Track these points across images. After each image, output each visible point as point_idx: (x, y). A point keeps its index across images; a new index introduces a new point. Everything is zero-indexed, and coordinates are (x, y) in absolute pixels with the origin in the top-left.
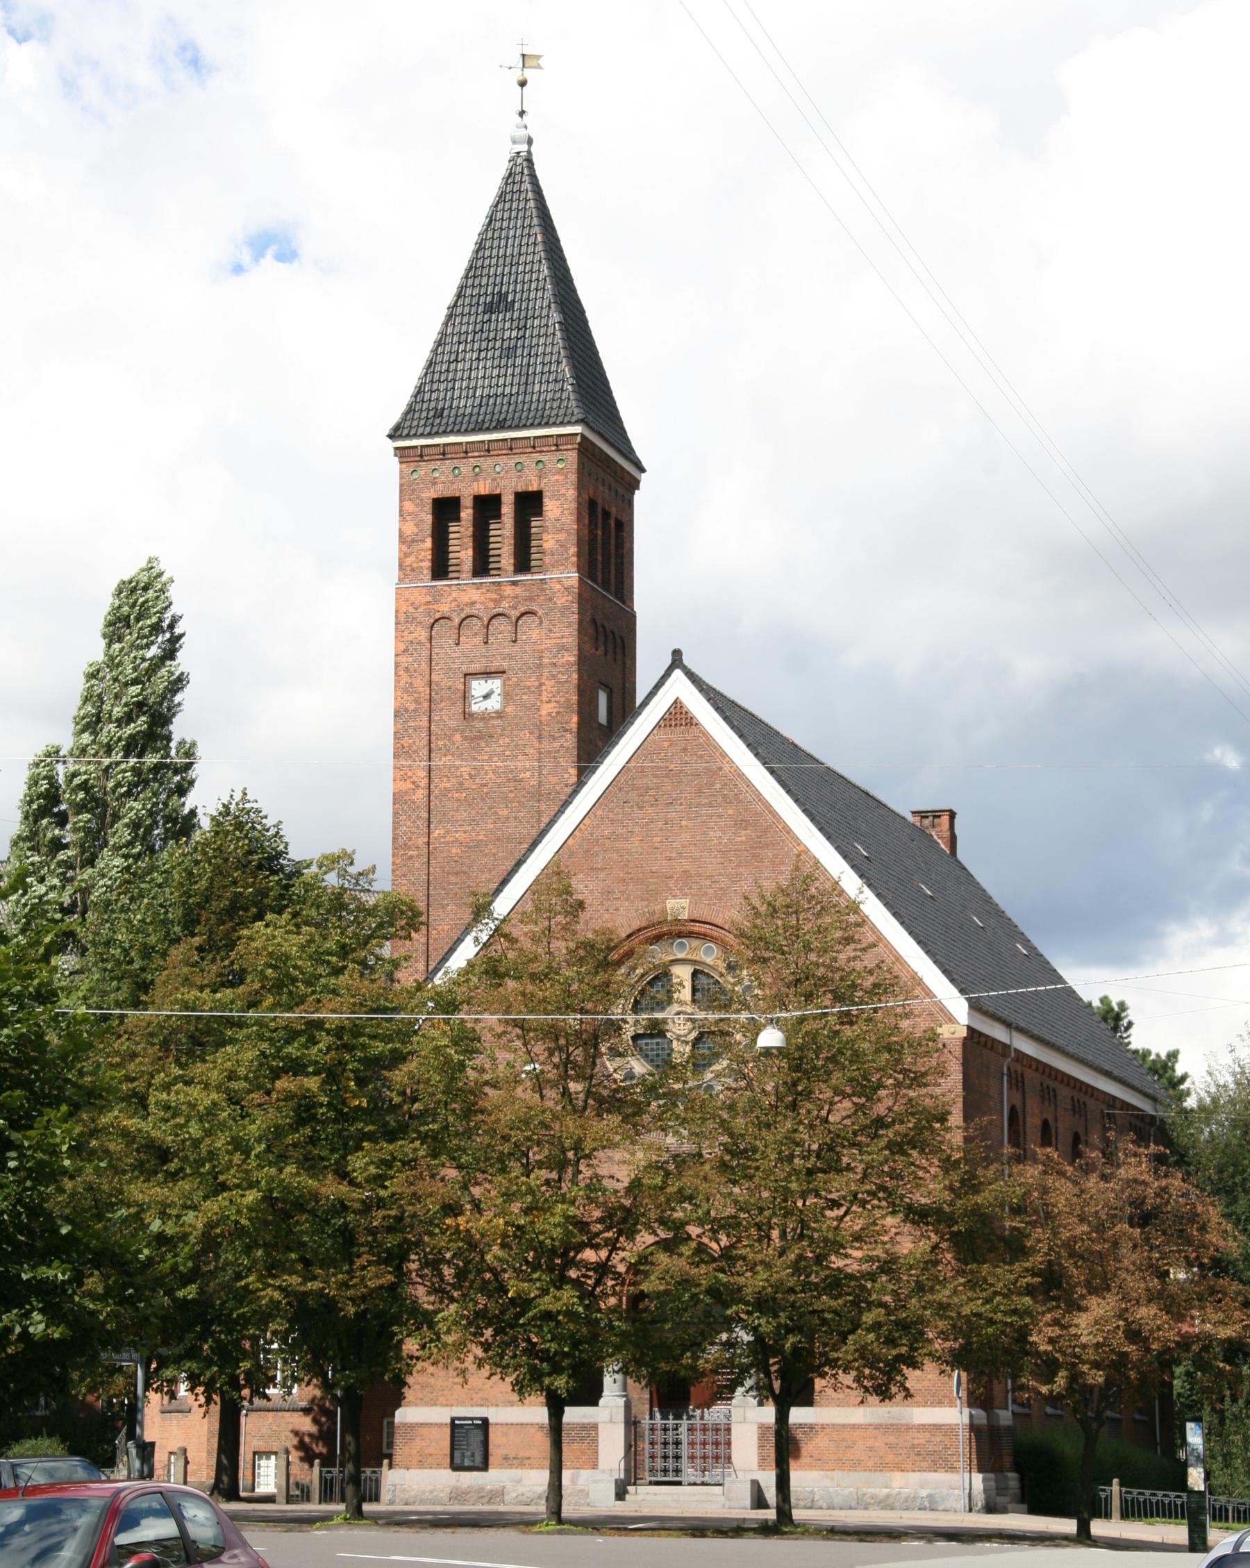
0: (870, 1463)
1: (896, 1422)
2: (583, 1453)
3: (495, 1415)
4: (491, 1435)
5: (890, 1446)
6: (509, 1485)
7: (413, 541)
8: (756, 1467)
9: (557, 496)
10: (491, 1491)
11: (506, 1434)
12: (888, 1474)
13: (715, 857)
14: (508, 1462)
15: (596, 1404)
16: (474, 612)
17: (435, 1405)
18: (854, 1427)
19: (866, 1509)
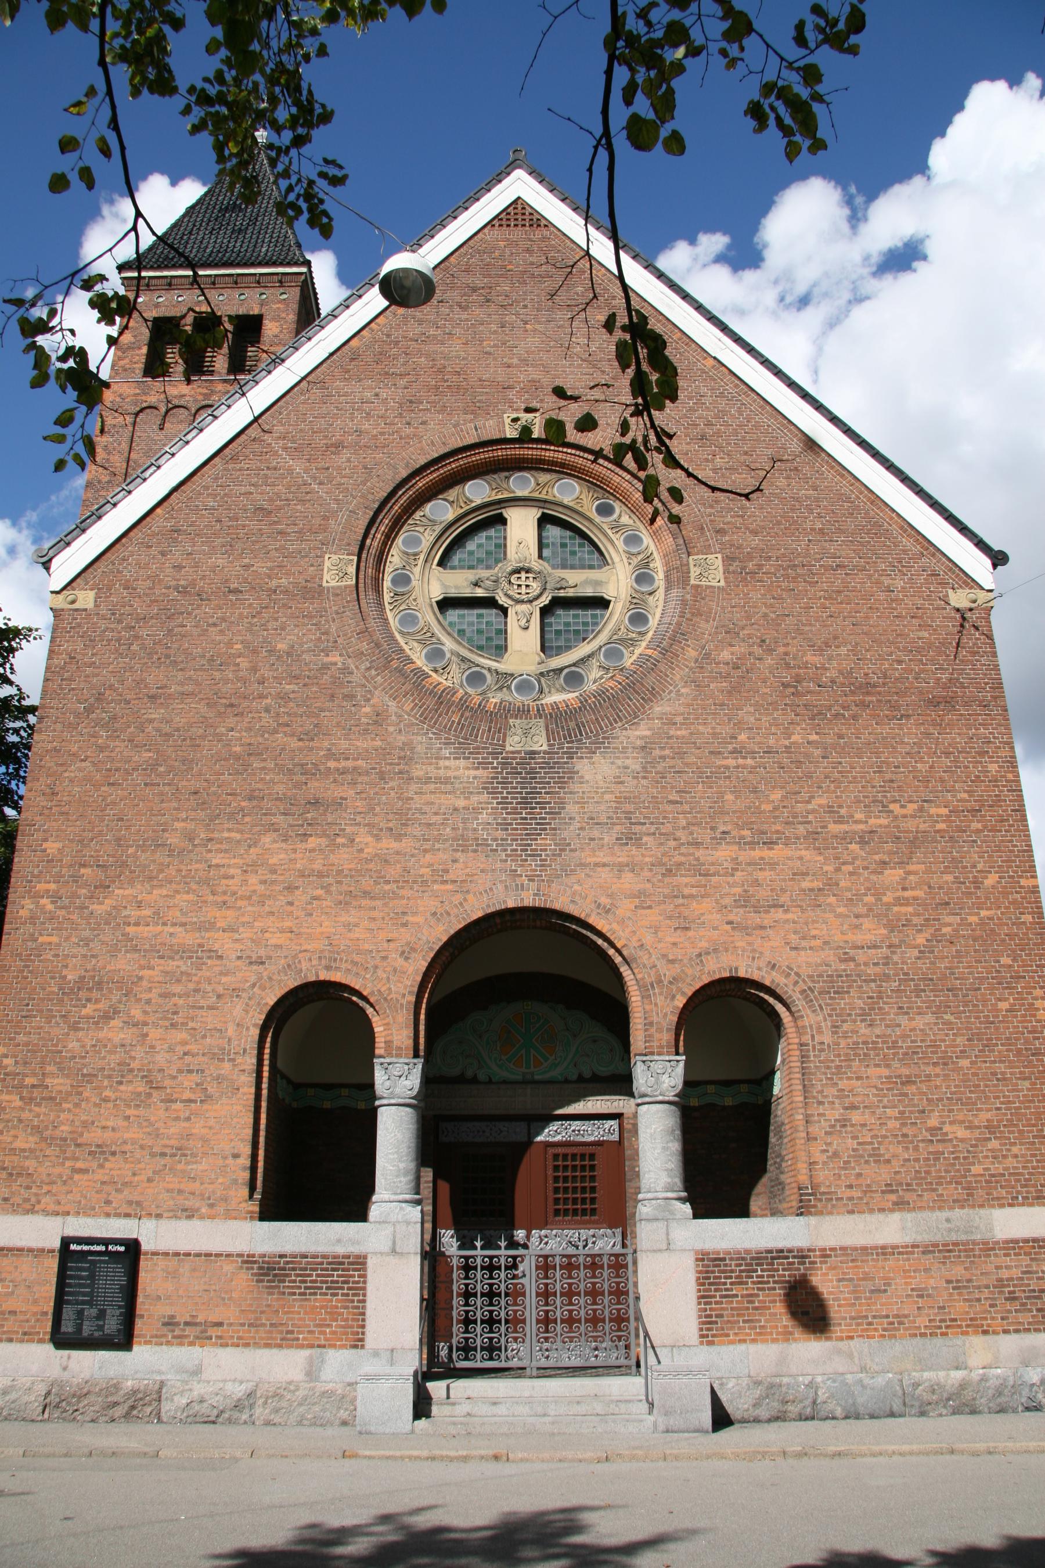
0: (922, 1321)
1: (963, 1237)
2: (334, 1315)
3: (153, 1235)
4: (143, 1276)
5: (957, 1285)
6: (172, 1378)
7: (129, 348)
8: (695, 1339)
9: (276, 319)
10: (135, 1392)
11: (174, 1275)
12: (959, 1340)
13: (579, 366)
14: (175, 1331)
15: (360, 1214)
16: (182, 403)
17: (31, 1211)
18: (884, 1251)
19: (923, 1414)
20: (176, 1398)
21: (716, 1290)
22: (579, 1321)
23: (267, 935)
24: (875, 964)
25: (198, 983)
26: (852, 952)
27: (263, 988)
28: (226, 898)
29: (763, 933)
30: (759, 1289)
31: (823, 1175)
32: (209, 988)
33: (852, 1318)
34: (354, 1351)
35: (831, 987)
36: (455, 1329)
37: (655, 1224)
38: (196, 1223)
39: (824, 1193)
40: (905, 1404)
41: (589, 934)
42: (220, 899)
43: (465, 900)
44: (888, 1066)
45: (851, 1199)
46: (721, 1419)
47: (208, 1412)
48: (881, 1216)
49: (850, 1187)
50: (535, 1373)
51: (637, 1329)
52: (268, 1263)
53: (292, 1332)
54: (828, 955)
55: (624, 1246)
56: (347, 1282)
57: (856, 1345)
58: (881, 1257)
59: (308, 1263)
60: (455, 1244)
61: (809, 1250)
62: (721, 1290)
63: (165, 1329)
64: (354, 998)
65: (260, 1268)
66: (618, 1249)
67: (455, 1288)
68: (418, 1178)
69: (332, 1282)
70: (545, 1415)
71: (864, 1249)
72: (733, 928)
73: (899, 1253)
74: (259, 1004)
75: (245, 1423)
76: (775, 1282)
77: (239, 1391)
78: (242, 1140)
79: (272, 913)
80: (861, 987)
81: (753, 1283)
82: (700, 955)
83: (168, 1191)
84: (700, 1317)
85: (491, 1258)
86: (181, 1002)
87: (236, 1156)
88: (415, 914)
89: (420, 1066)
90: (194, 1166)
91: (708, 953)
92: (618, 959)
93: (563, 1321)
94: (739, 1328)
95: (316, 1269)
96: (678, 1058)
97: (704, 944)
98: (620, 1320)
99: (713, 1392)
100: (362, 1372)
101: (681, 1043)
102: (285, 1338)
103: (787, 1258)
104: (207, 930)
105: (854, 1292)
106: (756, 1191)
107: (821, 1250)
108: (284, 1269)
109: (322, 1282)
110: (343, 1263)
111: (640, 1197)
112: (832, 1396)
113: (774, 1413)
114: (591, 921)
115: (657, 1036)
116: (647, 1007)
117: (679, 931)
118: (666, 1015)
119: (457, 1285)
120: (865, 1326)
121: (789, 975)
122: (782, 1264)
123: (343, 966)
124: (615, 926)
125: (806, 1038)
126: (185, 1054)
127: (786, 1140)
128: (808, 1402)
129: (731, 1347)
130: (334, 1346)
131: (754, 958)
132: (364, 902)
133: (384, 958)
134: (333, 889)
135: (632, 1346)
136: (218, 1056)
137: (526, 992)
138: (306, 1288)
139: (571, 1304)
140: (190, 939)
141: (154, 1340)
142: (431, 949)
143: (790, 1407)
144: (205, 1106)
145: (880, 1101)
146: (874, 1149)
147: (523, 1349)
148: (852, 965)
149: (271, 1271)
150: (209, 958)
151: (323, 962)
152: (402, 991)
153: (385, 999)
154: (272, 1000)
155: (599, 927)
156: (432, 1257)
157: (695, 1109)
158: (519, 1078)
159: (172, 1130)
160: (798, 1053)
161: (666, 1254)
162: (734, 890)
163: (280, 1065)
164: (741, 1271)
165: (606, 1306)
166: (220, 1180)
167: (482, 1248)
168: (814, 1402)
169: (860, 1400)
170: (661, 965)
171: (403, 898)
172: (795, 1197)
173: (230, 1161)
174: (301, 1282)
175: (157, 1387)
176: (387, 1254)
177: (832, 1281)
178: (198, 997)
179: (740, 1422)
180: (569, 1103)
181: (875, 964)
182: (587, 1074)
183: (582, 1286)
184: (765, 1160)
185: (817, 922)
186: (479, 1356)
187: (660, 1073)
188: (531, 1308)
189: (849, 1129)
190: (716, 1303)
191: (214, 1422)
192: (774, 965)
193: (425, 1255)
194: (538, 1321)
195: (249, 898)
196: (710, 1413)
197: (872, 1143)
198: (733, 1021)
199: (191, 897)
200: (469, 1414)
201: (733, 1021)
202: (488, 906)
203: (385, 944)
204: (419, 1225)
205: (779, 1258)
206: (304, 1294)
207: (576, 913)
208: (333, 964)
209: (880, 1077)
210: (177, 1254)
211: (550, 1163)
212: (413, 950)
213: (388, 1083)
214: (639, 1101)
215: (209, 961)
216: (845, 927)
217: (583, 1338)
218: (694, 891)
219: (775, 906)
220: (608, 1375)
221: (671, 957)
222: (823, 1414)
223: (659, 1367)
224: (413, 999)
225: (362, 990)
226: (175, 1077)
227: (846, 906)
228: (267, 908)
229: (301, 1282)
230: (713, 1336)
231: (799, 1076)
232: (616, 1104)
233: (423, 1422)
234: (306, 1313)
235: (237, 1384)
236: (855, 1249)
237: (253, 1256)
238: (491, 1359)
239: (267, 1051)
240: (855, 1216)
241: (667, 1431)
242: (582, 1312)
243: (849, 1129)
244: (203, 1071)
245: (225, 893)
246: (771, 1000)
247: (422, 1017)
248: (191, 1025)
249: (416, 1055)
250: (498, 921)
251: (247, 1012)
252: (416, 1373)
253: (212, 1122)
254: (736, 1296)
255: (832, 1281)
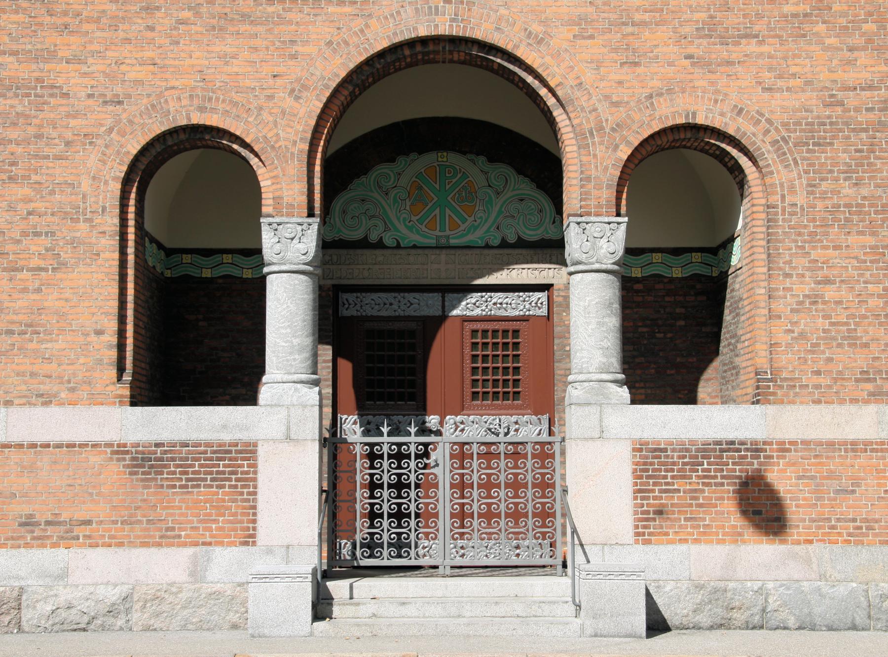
2: (221, 509)
18: (855, 447)
20: (38, 606)
21: (655, 484)
22: (498, 515)
23: (123, 68)
24: (867, 110)
25: (40, 126)
26: (840, 95)
27: (122, 134)
28: (67, 20)
29: (730, 70)
30: (704, 484)
31: (786, 360)
32: (54, 134)
33: (813, 520)
34: (244, 548)
35: (813, 136)
36: (358, 524)
37: (587, 409)
38: (53, 410)
39: (786, 379)
40: (869, 617)
41: (516, 69)
42: (60, 22)
43: (367, 26)
44: (874, 234)
45: (817, 387)
46: (657, 625)
47: (77, 619)
48: (853, 408)
49: (818, 373)
50: (448, 571)
51: (564, 526)
52: (143, 453)
53: (173, 529)
54: (811, 98)
55: (551, 433)
56: (235, 473)
57: (815, 549)
58: (850, 454)
59: (189, 452)
60: (358, 429)
61: (765, 443)
62: (661, 484)
63: (23, 529)
64: (235, 146)
65: (133, 459)
66: (545, 437)
67: (358, 478)
68: (315, 355)
69: (218, 473)
70: (459, 616)
71: (831, 444)
72: (693, 64)
73: (872, 450)
74: (118, 153)
75: (121, 629)
76: (723, 477)
77: (112, 595)
78: (106, 314)
79: (128, 41)
80: (849, 137)
81: (698, 477)
82: (651, 96)
83: (18, 375)
84: (636, 513)
85: (399, 445)
86: (19, 150)
87: (99, 333)
88: (306, 43)
89: (315, 227)
90: (49, 345)
91: (660, 95)
92: (551, 101)
93: (480, 516)
94: (680, 527)
95: (198, 459)
96: (619, 219)
97: (656, 83)
98: (545, 515)
99: (648, 594)
100: (254, 571)
101: (624, 202)
102: (167, 537)
103: (739, 450)
104: (46, 61)
105: (816, 491)
106: (705, 376)
107: (778, 443)
108: (161, 459)
109: (206, 473)
110: (230, 452)
111: (571, 378)
112: (784, 604)
113: (718, 621)
114: (519, 53)
115: (594, 192)
116: (584, 159)
117: (626, 68)
118: (606, 168)
119: (361, 476)
120: (828, 531)
121: (758, 122)
122: (733, 457)
123: (220, 107)
124: (548, 59)
125: (776, 199)
126: (30, 213)
127: (743, 318)
128: (755, 610)
129: (670, 547)
130: (221, 544)
131: (716, 101)
132: (244, 28)
133: (270, 97)
134: (204, 10)
135: (558, 544)
136: (72, 216)
137: (441, 135)
138: (188, 480)
139: (489, 496)
140: (25, 72)
141: (10, 542)
142: (337, 75)
143: (735, 614)
144: (59, 275)
145: (862, 275)
146: (849, 331)
147: (436, 546)
148: (839, 109)
149: (146, 461)
150: (52, 95)
151: (195, 101)
152: (292, 137)
153: (273, 147)
154: (134, 148)
155: (529, 61)
156: (332, 444)
157: (637, 280)
158: (432, 242)
159: (19, 303)
160: (763, 216)
161: (598, 443)
162: (697, 16)
163: (148, 226)
164: (684, 464)
165: (530, 500)
166: (81, 361)
167: (390, 434)
168: (764, 610)
169: (817, 610)
170: (603, 109)
171: (290, 22)
172: (752, 383)
173: (93, 338)
174: (181, 473)
175: (15, 593)
176: (281, 441)
177: (790, 478)
178: (41, 144)
179: (677, 628)
180: (491, 271)
181: (867, 110)
182: (512, 239)
183: (502, 478)
184: (718, 341)
185: (799, 57)
186: (385, 553)
187: (597, 238)
188: (444, 501)
189: (820, 306)
190: (655, 498)
191: (84, 630)
192: (741, 110)
193: (324, 442)
194: (452, 516)
195: (98, 21)
196: (644, 617)
197: (847, 324)
198: (689, 175)
199: (20, 17)
200: (374, 615)
201: (689, 175)
202: (395, 34)
203: (271, 81)
204: (317, 408)
205: (728, 450)
206: (186, 487)
207: (501, 44)
208: (207, 105)
209: (864, 247)
210: (33, 446)
211: (468, 341)
212: (305, 87)
213: (278, 247)
214: (572, 269)
215: (52, 100)
216: (835, 62)
217: (503, 535)
218: (647, 17)
219: (746, 36)
220: (531, 575)
221: (615, 99)
222: (773, 623)
223: (587, 566)
224: (306, 147)
225: (243, 136)
226: (19, 242)
227: (837, 36)
228: (121, 34)
229: (181, 473)
230: (650, 534)
231: (764, 243)
232: (544, 273)
233: (320, 625)
234: (187, 508)
235: (110, 588)
236: (820, 443)
237: (125, 445)
238: (399, 556)
239: (132, 209)
240: (822, 406)
241: (596, 636)
242: (503, 506)
243: (820, 306)
244: (53, 234)
245: (65, 13)
246: (734, 152)
247: (318, 169)
248: (34, 178)
249: (311, 214)
250: (407, 52)
251: (104, 162)
252: (315, 571)
253: (68, 294)
254: (678, 491)
255: (790, 478)
